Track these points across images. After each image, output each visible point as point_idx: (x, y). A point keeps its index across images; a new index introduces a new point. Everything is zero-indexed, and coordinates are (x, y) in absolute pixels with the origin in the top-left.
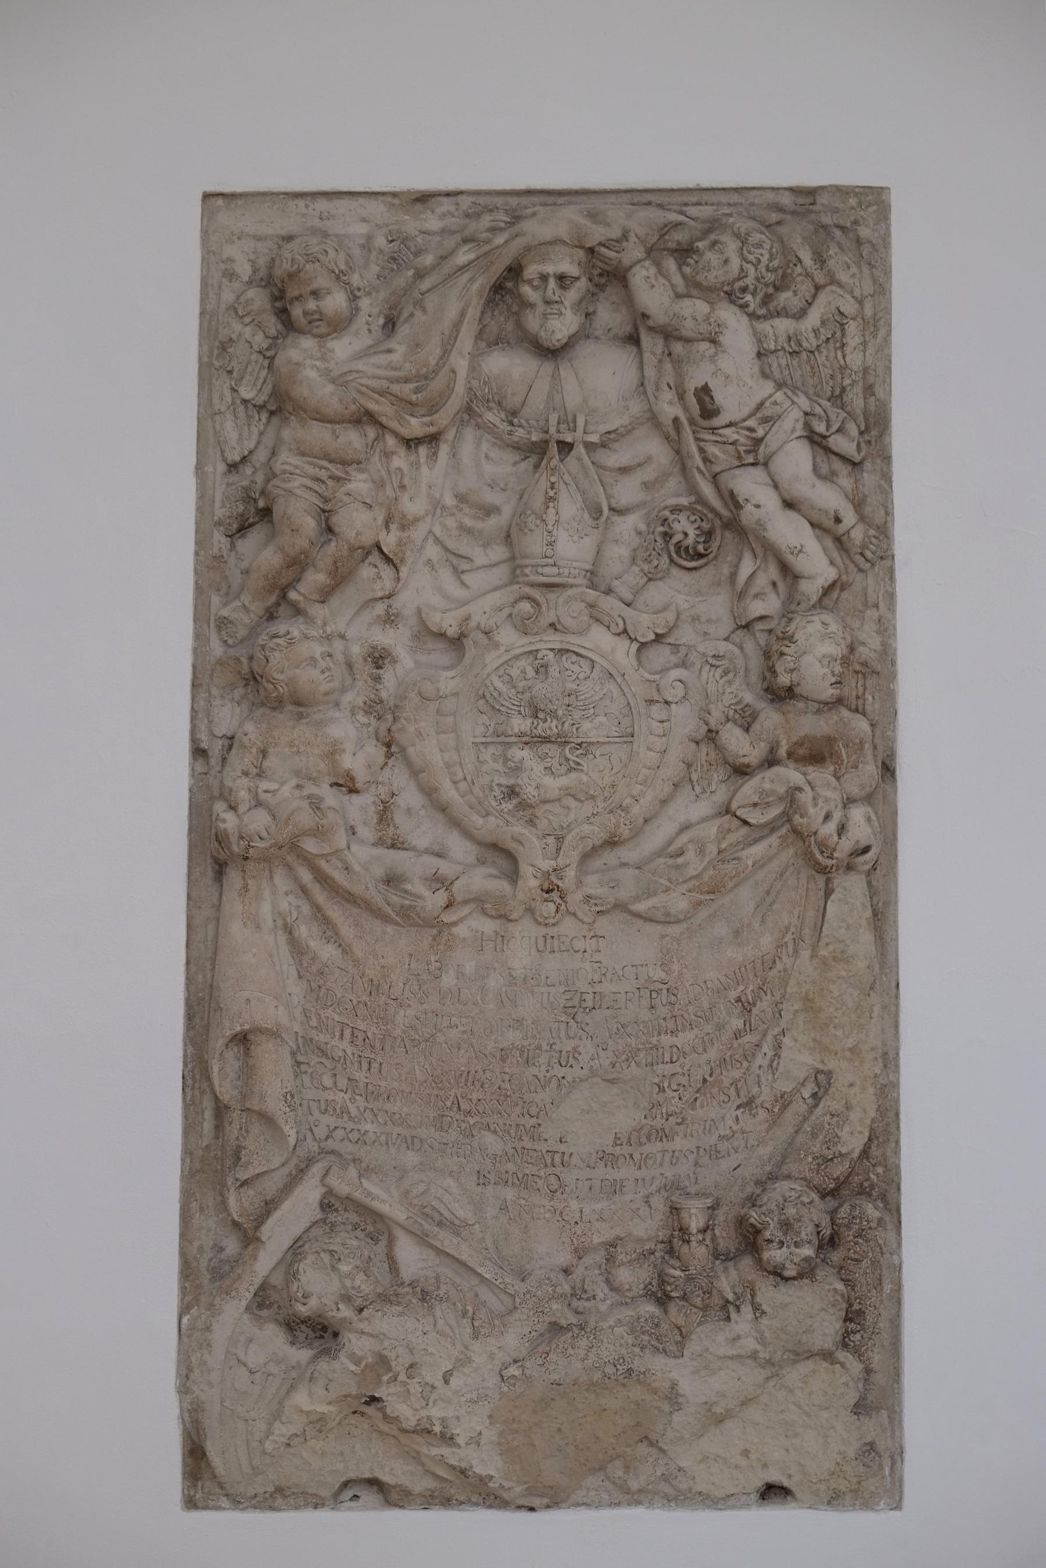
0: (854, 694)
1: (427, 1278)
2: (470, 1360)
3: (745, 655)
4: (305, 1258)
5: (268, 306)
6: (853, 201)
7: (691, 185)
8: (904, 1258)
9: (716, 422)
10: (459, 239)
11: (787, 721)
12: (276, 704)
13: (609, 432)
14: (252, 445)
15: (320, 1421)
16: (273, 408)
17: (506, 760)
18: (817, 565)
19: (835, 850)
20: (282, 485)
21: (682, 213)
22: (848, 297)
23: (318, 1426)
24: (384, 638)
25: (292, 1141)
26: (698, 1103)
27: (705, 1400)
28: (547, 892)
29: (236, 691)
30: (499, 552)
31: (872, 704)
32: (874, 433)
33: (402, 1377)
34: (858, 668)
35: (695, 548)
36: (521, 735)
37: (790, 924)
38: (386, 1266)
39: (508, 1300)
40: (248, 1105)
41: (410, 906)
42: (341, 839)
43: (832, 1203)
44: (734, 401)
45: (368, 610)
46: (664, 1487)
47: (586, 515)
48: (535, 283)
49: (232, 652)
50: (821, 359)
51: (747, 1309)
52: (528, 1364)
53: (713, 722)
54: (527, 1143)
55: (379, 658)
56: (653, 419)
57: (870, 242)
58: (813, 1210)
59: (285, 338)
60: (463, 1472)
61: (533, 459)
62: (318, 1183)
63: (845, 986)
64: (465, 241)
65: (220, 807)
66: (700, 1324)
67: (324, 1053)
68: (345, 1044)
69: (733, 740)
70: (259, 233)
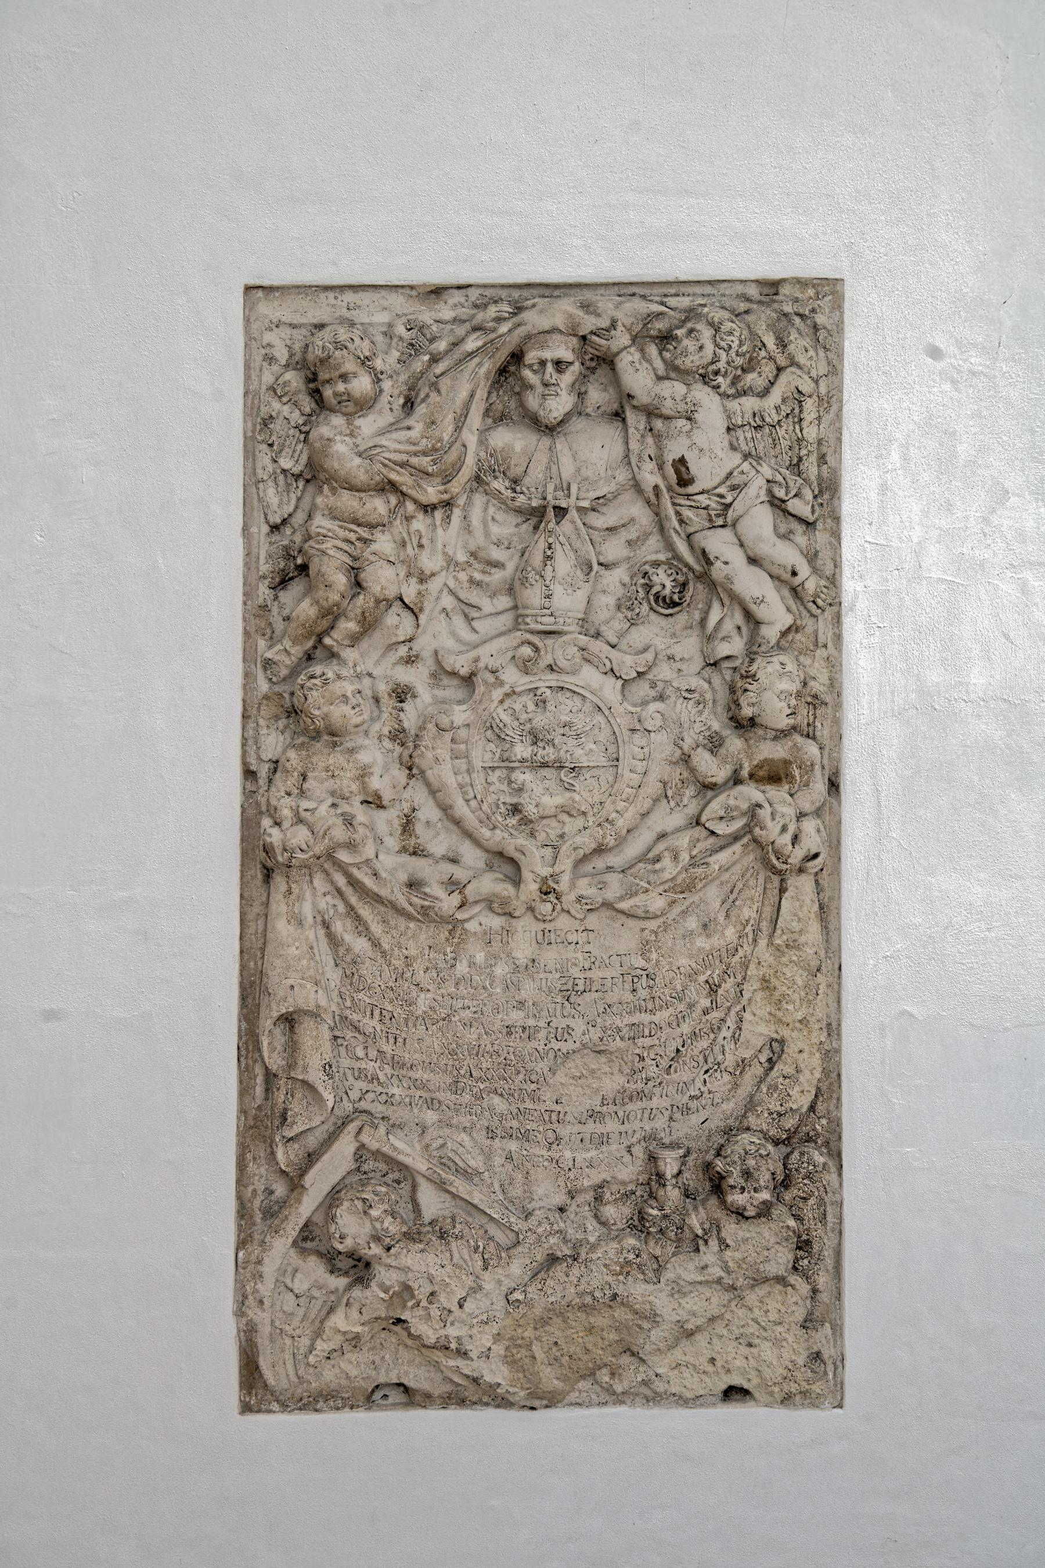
0: (806, 722)
1: (444, 1218)
2: (480, 1288)
3: (713, 688)
4: (341, 1204)
5: (303, 388)
6: (811, 292)
7: (671, 279)
8: (845, 1197)
9: (690, 490)
10: (469, 327)
11: (749, 747)
12: (314, 734)
13: (598, 498)
14: (291, 509)
15: (355, 1341)
16: (309, 477)
17: (510, 782)
18: (776, 613)
19: (789, 857)
20: (317, 546)
21: (662, 304)
22: (806, 377)
23: (353, 1343)
24: (405, 675)
25: (330, 1104)
26: (672, 1069)
27: (678, 1318)
28: (545, 894)
29: (280, 722)
30: (504, 602)
31: (823, 731)
32: (826, 496)
33: (424, 1303)
34: (809, 699)
35: (671, 598)
36: (523, 761)
37: (750, 918)
38: (410, 1206)
39: (512, 1236)
40: (293, 1075)
41: (429, 907)
42: (369, 851)
43: (784, 1149)
44: (706, 472)
45: (393, 652)
46: (644, 1390)
47: (579, 572)
48: (535, 367)
49: (277, 689)
50: (781, 432)
51: (714, 1244)
52: (529, 1289)
53: (686, 747)
54: (529, 1105)
55: (402, 694)
56: (637, 487)
57: (825, 328)
58: (769, 1161)
59: (318, 416)
60: (475, 1380)
61: (534, 521)
62: (353, 1139)
63: (796, 969)
64: (475, 329)
65: (266, 822)
66: (674, 1255)
67: (357, 1029)
68: (375, 1022)
69: (703, 763)
70: (295, 322)
